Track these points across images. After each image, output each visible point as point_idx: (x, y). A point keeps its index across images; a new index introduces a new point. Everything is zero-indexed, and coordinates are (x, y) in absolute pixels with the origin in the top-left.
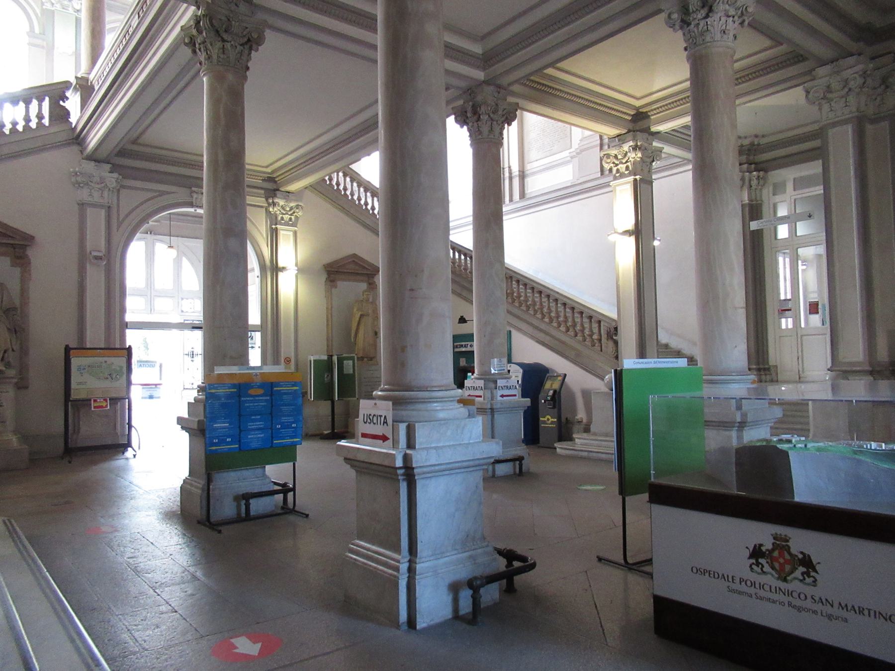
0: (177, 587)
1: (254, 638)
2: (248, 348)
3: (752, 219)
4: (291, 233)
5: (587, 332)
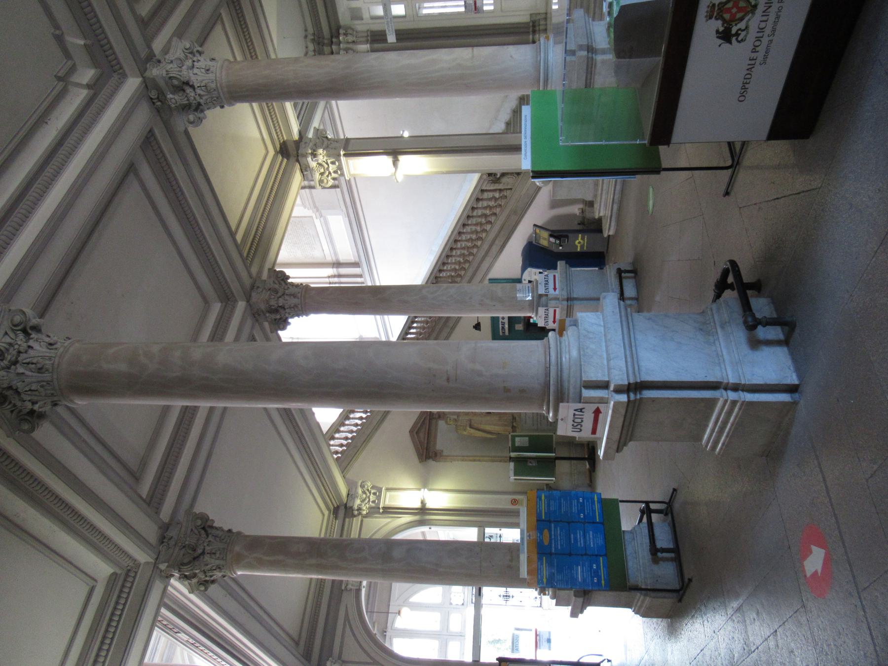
0: (749, 628)
1: (807, 553)
2: (506, 587)
3: (385, 40)
4: (388, 494)
5: (492, 203)
